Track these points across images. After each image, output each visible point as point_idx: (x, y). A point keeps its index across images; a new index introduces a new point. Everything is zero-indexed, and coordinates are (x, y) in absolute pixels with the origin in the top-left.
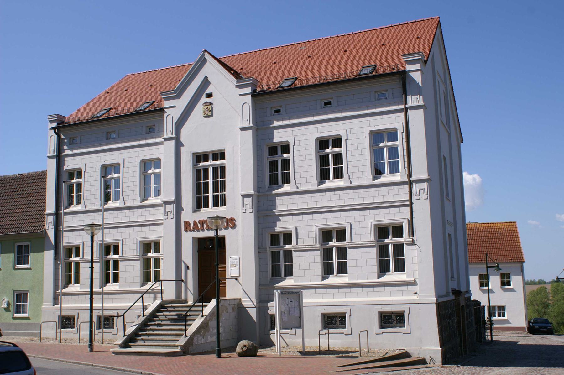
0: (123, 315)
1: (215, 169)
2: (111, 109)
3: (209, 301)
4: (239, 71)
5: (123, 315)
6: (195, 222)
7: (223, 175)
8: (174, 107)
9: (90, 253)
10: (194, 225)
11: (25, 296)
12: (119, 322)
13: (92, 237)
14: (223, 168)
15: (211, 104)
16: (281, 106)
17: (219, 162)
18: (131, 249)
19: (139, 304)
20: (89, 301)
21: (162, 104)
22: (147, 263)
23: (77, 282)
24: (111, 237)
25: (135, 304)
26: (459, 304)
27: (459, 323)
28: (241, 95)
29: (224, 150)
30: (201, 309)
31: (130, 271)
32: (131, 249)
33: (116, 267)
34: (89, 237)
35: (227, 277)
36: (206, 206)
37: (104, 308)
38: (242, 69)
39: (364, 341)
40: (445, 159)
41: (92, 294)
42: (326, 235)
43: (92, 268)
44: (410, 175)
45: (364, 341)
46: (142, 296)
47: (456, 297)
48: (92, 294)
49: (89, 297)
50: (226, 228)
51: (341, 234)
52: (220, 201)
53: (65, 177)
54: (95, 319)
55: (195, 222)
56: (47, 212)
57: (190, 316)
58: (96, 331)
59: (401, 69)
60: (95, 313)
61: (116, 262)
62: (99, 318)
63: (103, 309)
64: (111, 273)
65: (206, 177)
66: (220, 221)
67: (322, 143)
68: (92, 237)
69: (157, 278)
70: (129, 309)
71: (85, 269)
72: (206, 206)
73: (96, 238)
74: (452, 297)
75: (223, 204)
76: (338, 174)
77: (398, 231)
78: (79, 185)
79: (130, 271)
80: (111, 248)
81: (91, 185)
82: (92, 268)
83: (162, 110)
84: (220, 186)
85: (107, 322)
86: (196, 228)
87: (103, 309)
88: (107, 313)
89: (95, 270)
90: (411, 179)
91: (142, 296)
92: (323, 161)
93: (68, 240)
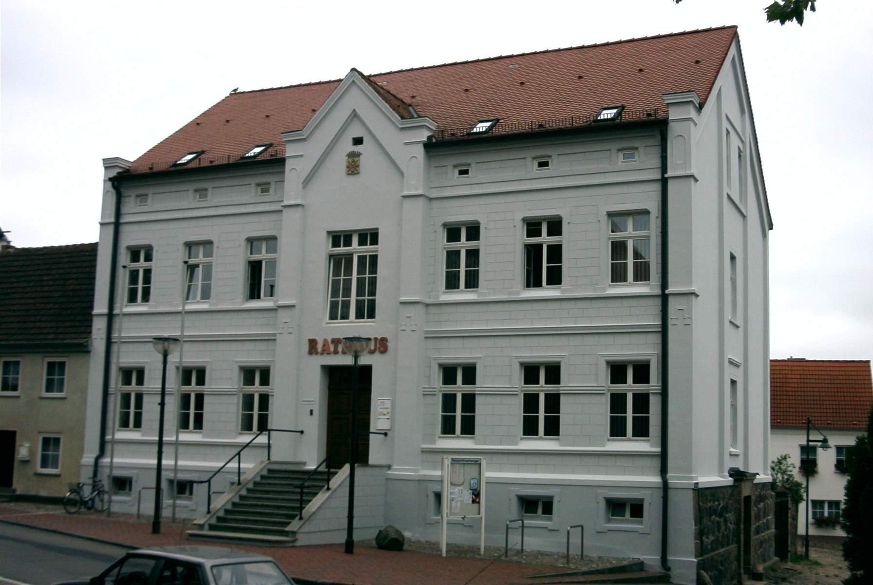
0: (209, 481)
1: (362, 259)
2: (203, 152)
3: (340, 468)
4: (408, 100)
5: (209, 481)
6: (325, 341)
7: (334, 305)
8: (301, 156)
9: (160, 381)
10: (324, 345)
11: (57, 441)
12: (200, 491)
13: (165, 356)
14: (374, 259)
15: (358, 155)
16: (469, 165)
17: (369, 248)
18: (224, 380)
19: (234, 465)
20: (156, 455)
21: (284, 151)
22: (248, 401)
23: (138, 424)
24: (192, 357)
25: (228, 465)
26: (740, 493)
27: (737, 523)
28: (406, 144)
29: (377, 229)
30: (326, 477)
31: (223, 413)
32: (224, 380)
33: (200, 404)
34: (160, 357)
35: (372, 430)
36: (345, 316)
37: (114, 465)
38: (413, 97)
39: (575, 540)
40: (733, 258)
41: (160, 443)
42: (530, 372)
43: (162, 404)
44: (664, 285)
45: (575, 540)
46: (239, 454)
47: (735, 481)
48: (160, 443)
49: (155, 449)
50: (372, 352)
51: (554, 372)
52: (367, 310)
53: (124, 258)
54: (164, 485)
55: (325, 341)
56: (96, 311)
57: (308, 487)
58: (166, 502)
59: (661, 115)
60: (165, 475)
61: (200, 398)
62: (171, 482)
63: (176, 469)
64: (193, 414)
65: (348, 271)
66: (364, 343)
67: (533, 227)
68: (165, 356)
69: (263, 427)
70: (219, 471)
71: (150, 407)
72: (345, 316)
73: (170, 358)
74: (729, 481)
75: (372, 315)
76: (555, 278)
77: (642, 372)
78: (148, 272)
79: (223, 413)
80: (194, 375)
81: (167, 271)
82: (162, 404)
83: (281, 162)
84: (369, 287)
85: (183, 487)
86: (325, 351)
87: (176, 469)
88: (182, 476)
89: (167, 408)
90: (667, 292)
91: (239, 454)
92: (533, 253)
93: (126, 357)
